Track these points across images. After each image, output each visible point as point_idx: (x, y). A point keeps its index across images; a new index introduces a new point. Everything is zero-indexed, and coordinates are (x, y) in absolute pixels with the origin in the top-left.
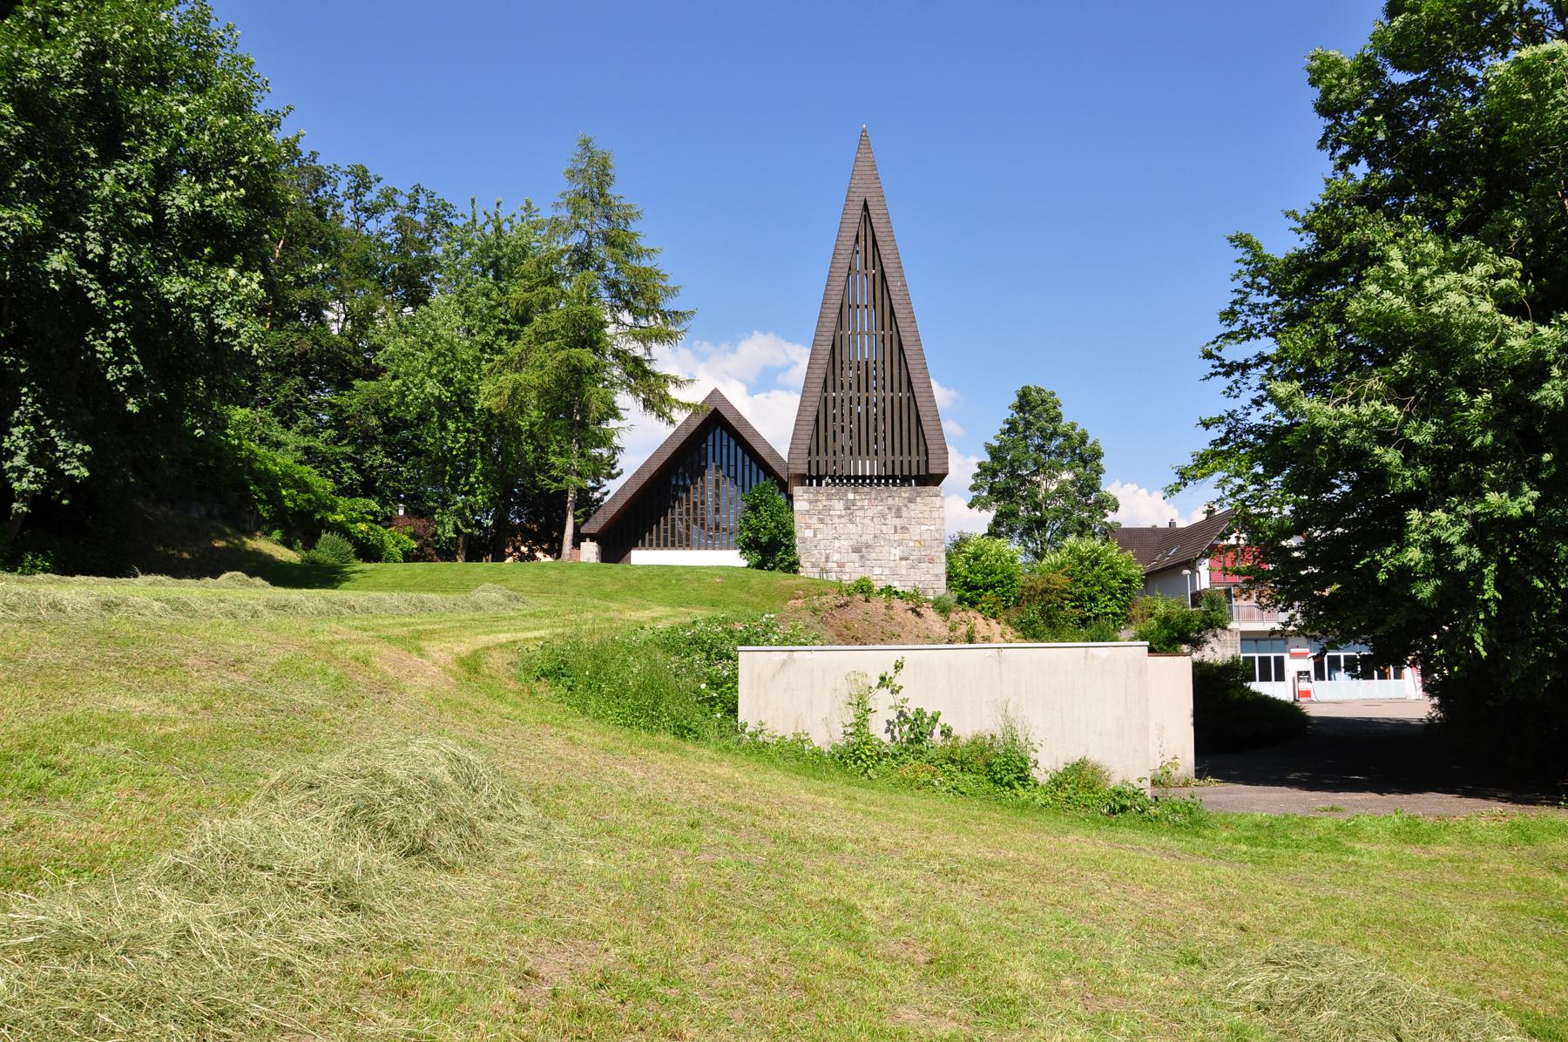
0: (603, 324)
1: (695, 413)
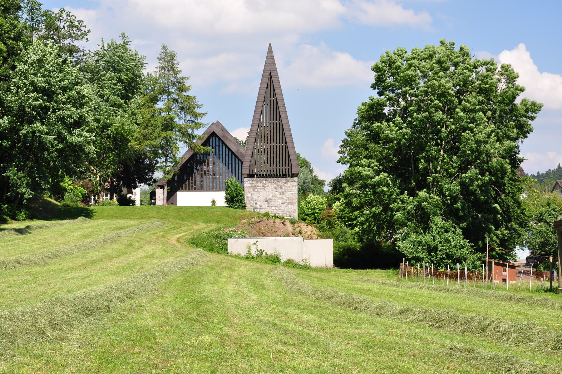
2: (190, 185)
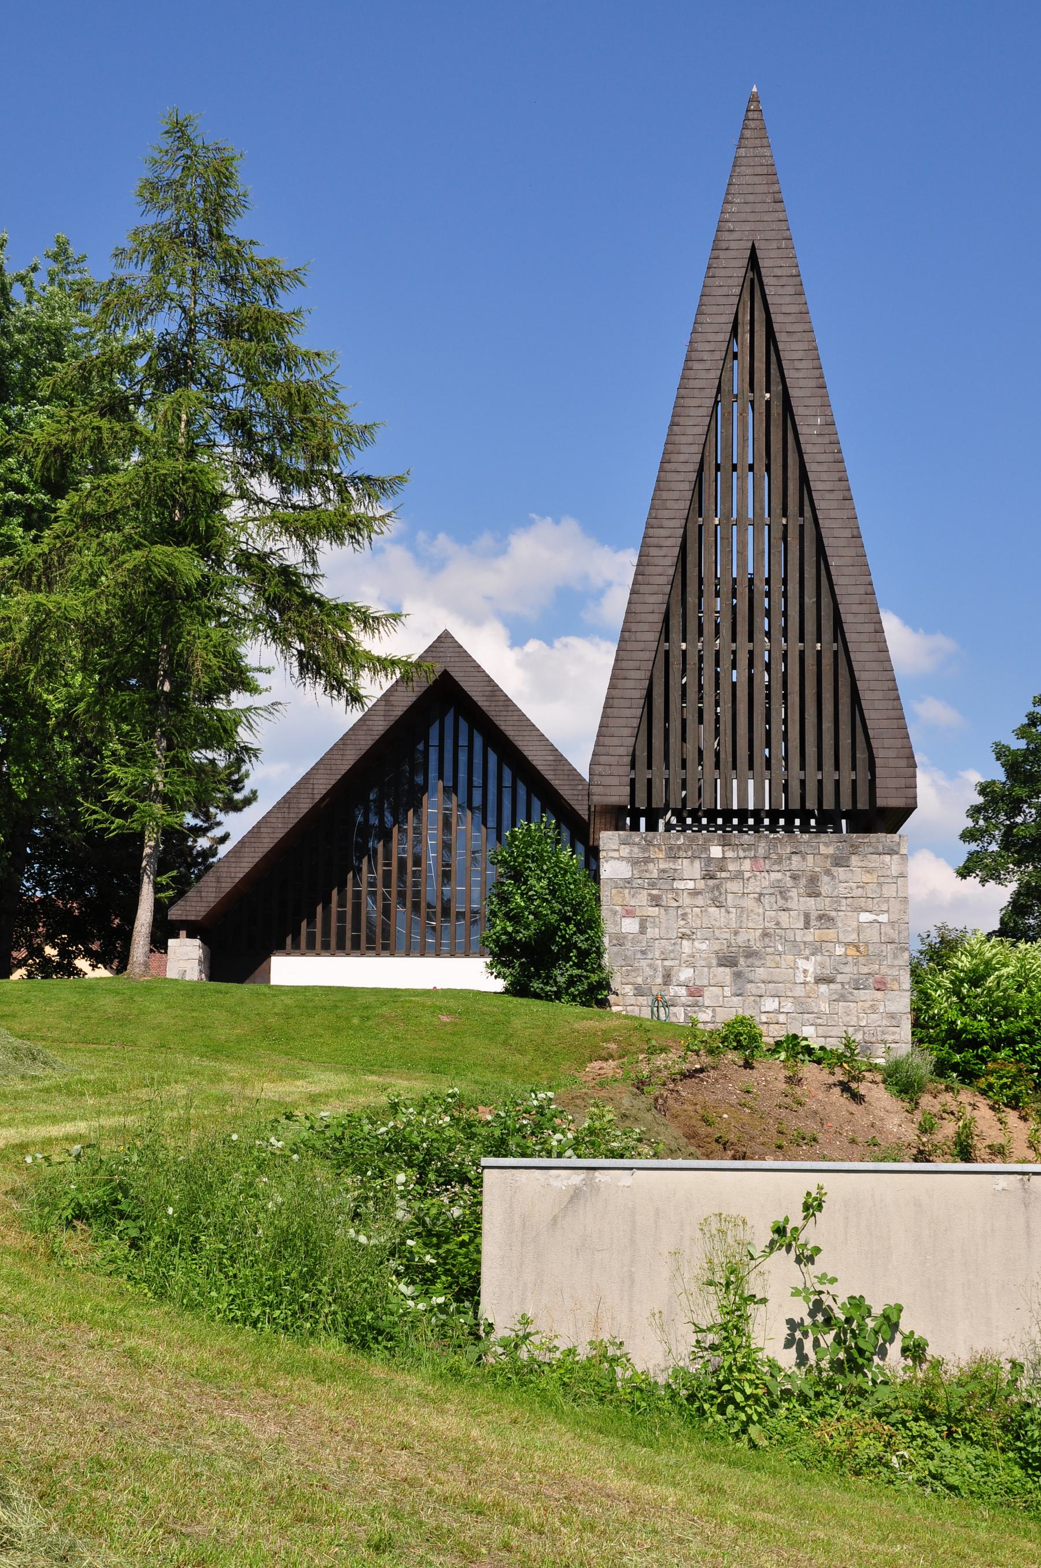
0: (219, 500)
1: (406, 679)
2: (334, 924)
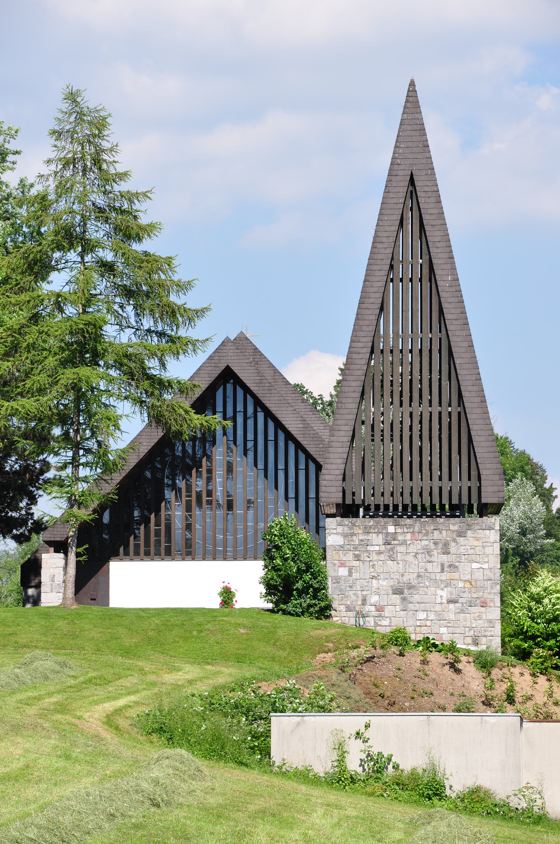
2: (153, 538)
